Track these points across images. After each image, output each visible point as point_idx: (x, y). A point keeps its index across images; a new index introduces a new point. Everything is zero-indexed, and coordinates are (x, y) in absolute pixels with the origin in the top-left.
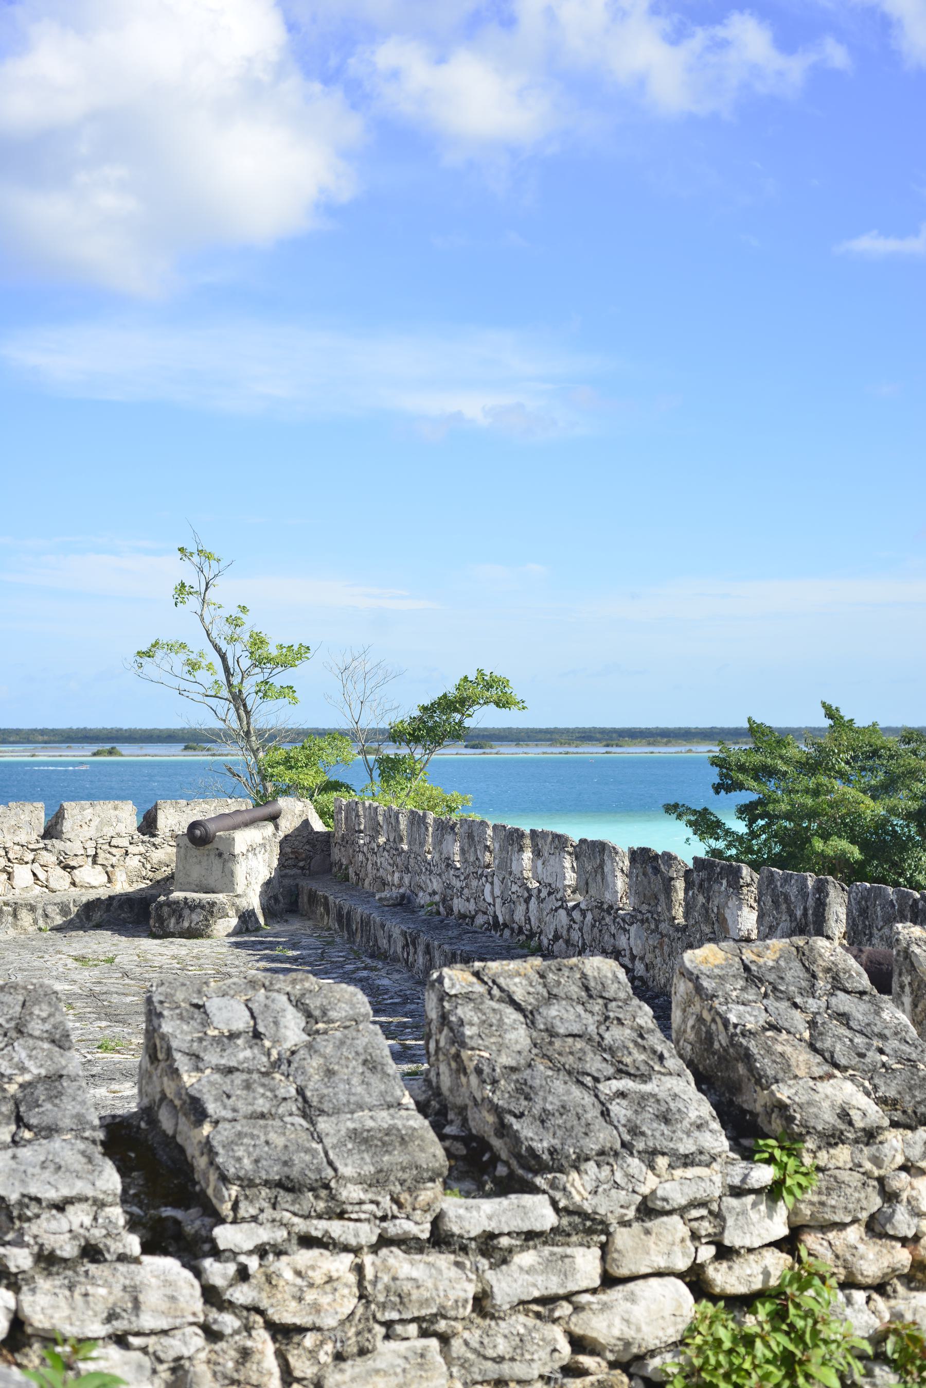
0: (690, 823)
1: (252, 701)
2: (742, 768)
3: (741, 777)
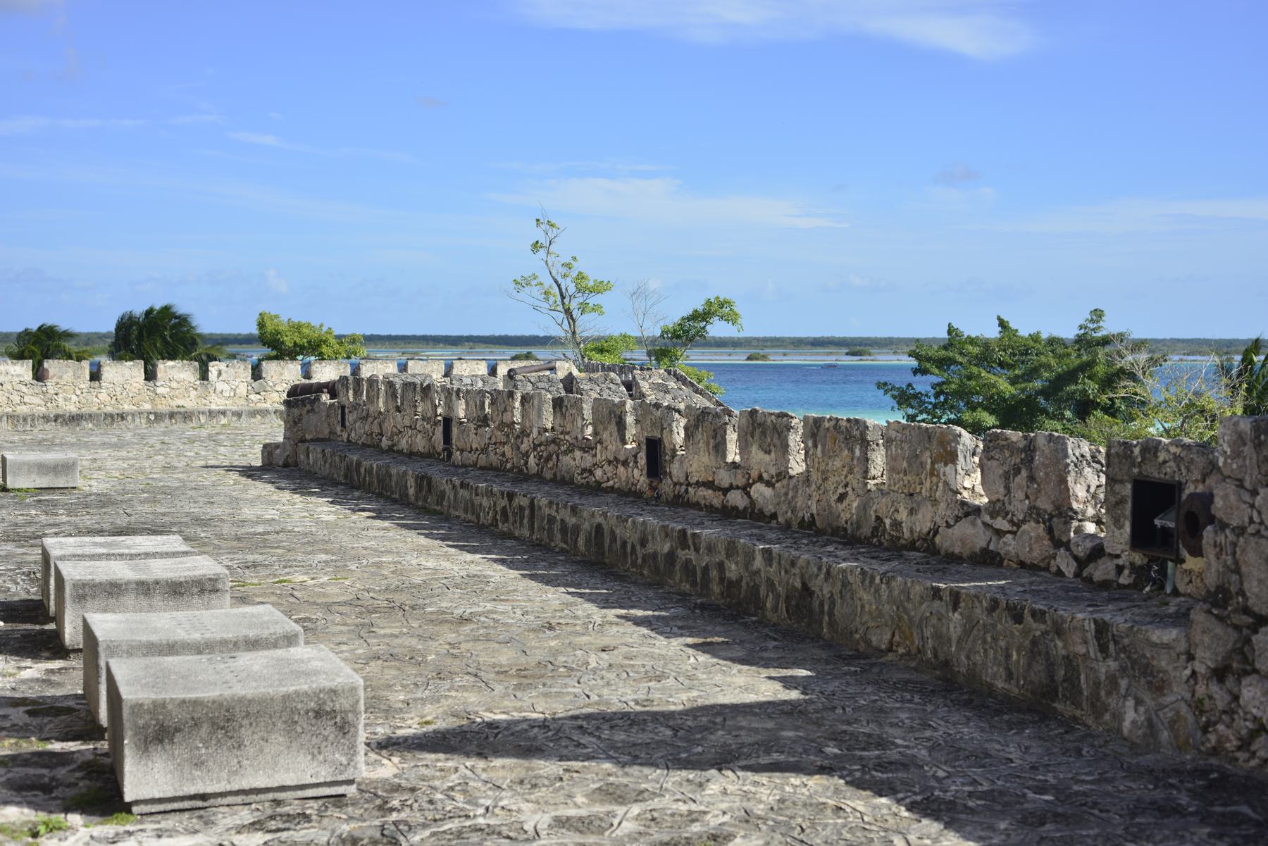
0: (894, 397)
1: (576, 314)
2: (929, 359)
3: (928, 365)
